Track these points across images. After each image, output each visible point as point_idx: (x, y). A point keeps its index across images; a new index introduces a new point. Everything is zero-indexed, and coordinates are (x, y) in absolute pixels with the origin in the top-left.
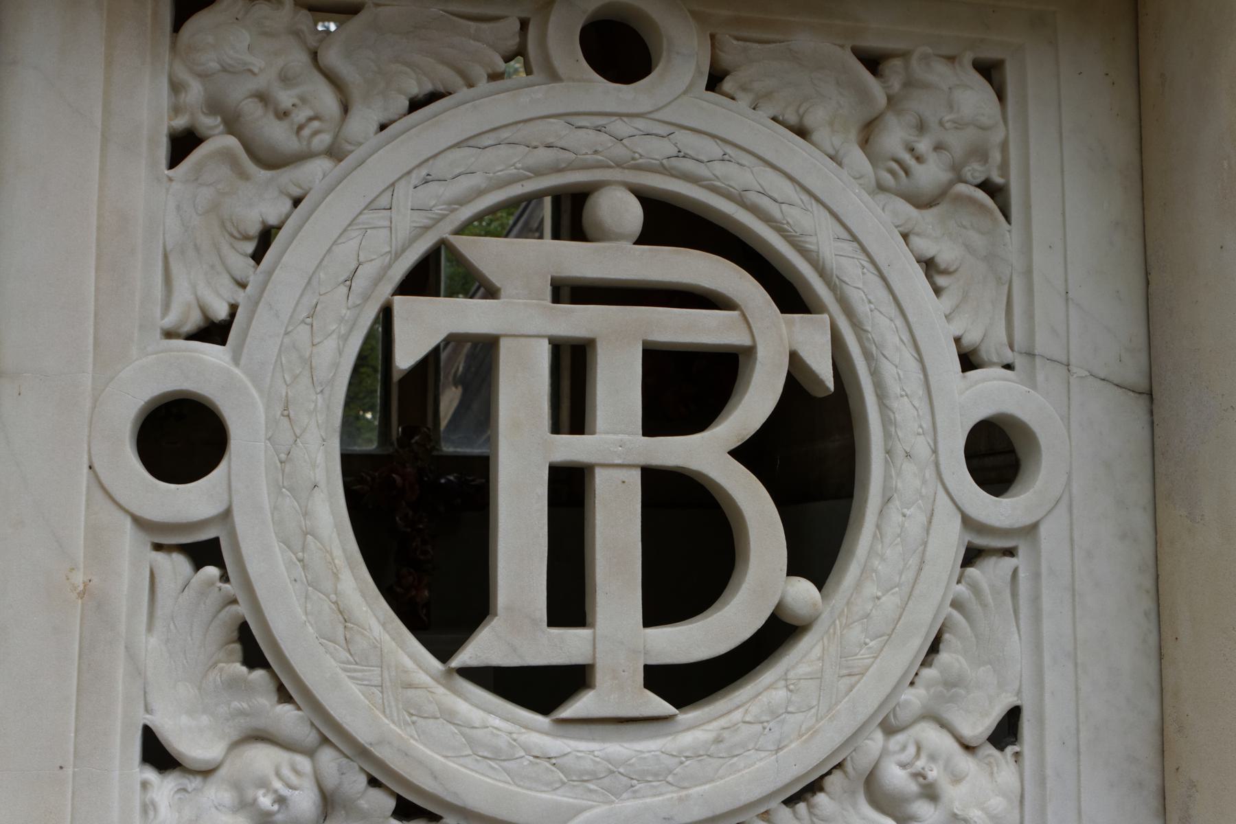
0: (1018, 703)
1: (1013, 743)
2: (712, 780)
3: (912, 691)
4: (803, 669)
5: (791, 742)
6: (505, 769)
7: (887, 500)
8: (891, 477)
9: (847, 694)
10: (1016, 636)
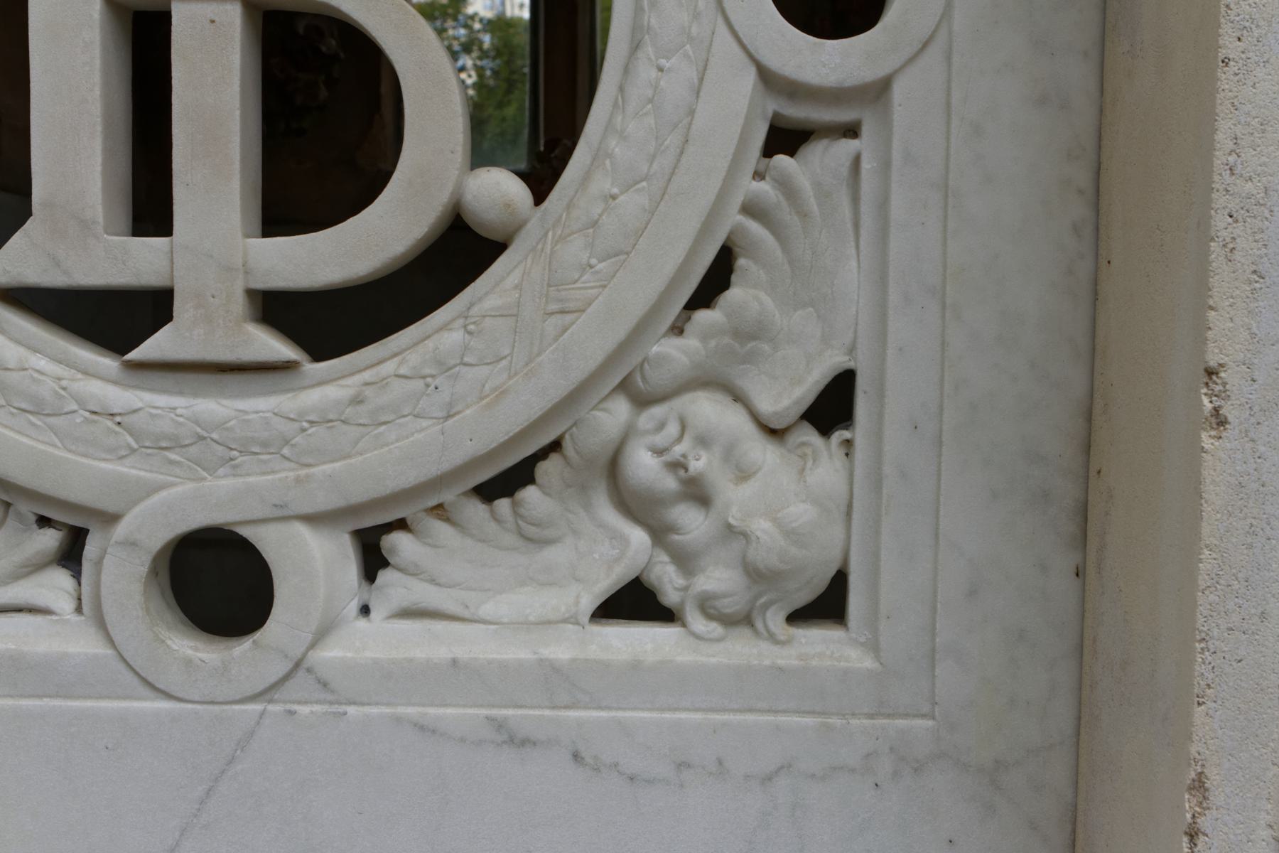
0: (851, 365)
1: (846, 428)
2: (348, 456)
3: (676, 341)
4: (491, 302)
5: (468, 407)
6: (51, 428)
7: (636, 47)
8: (642, 9)
9: (556, 339)
10: (854, 263)
